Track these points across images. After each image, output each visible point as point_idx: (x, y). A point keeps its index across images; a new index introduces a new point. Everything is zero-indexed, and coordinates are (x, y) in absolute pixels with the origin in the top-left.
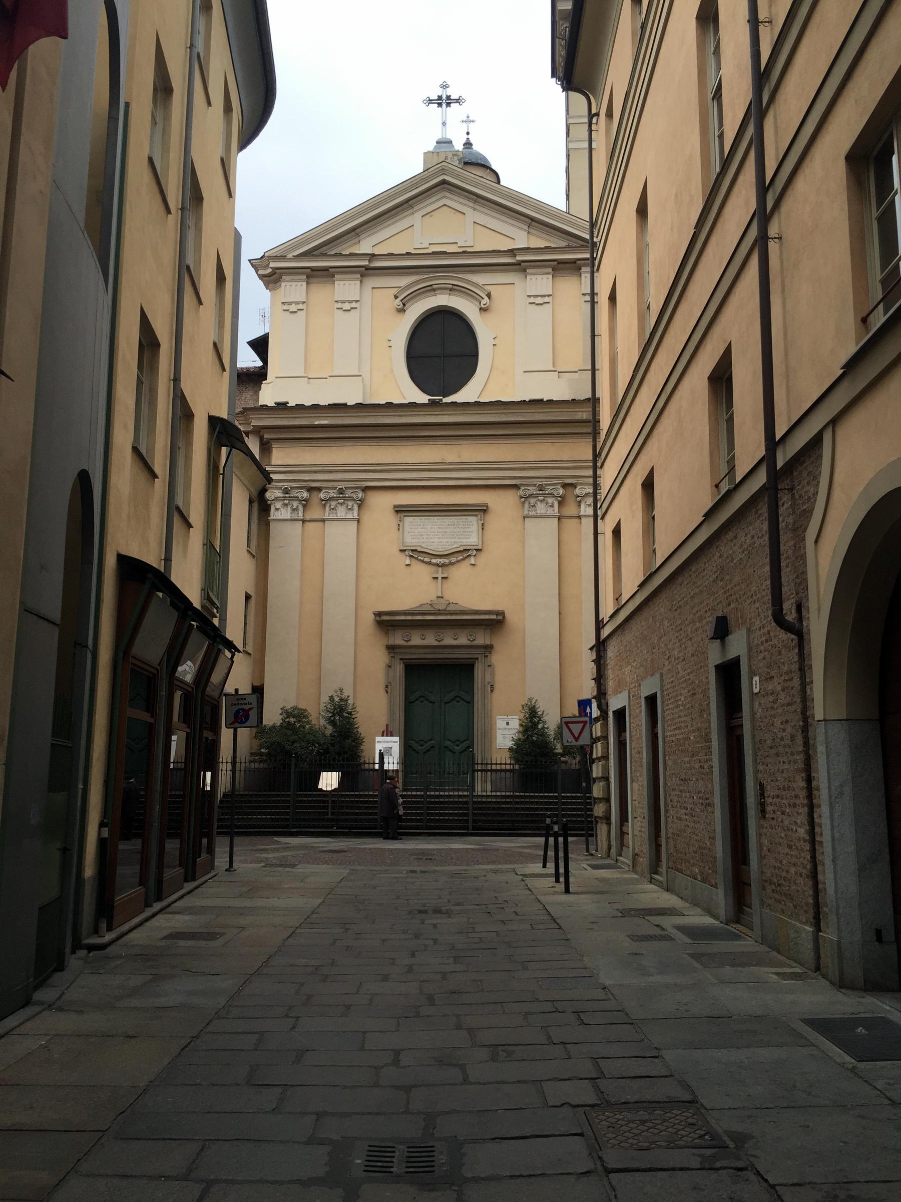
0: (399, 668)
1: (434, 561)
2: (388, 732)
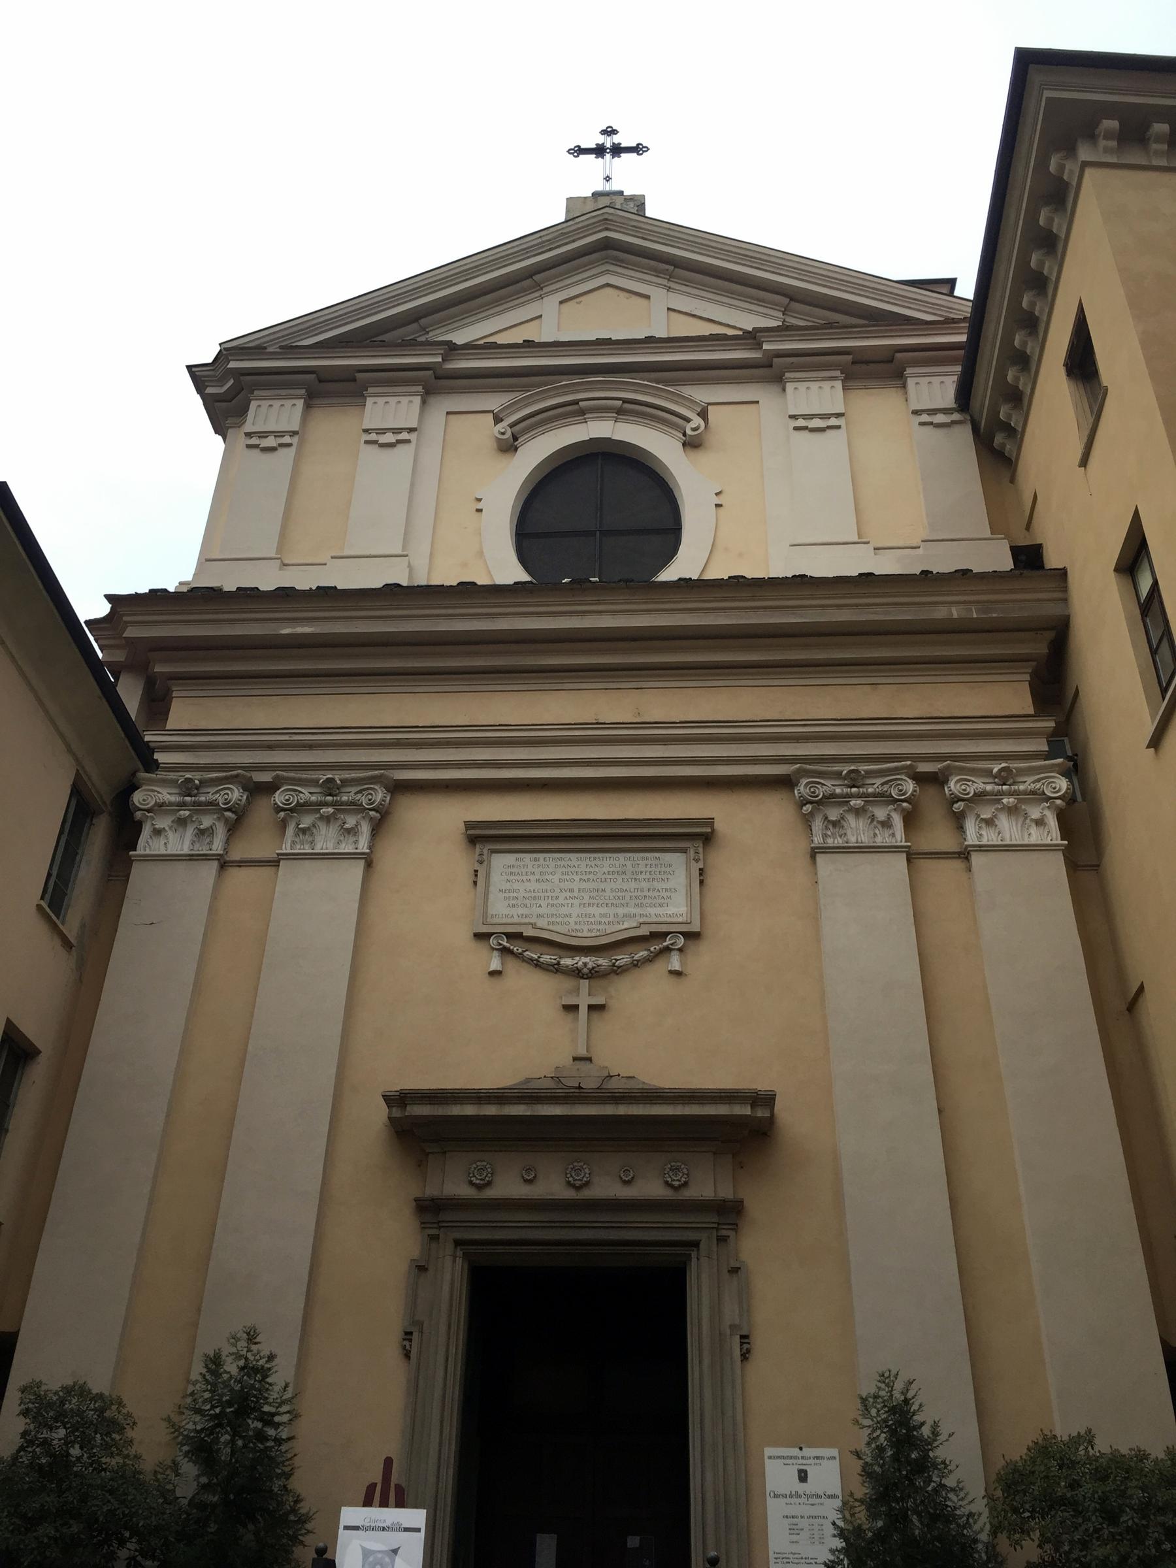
0: (451, 1275)
1: (567, 962)
2: (386, 1492)
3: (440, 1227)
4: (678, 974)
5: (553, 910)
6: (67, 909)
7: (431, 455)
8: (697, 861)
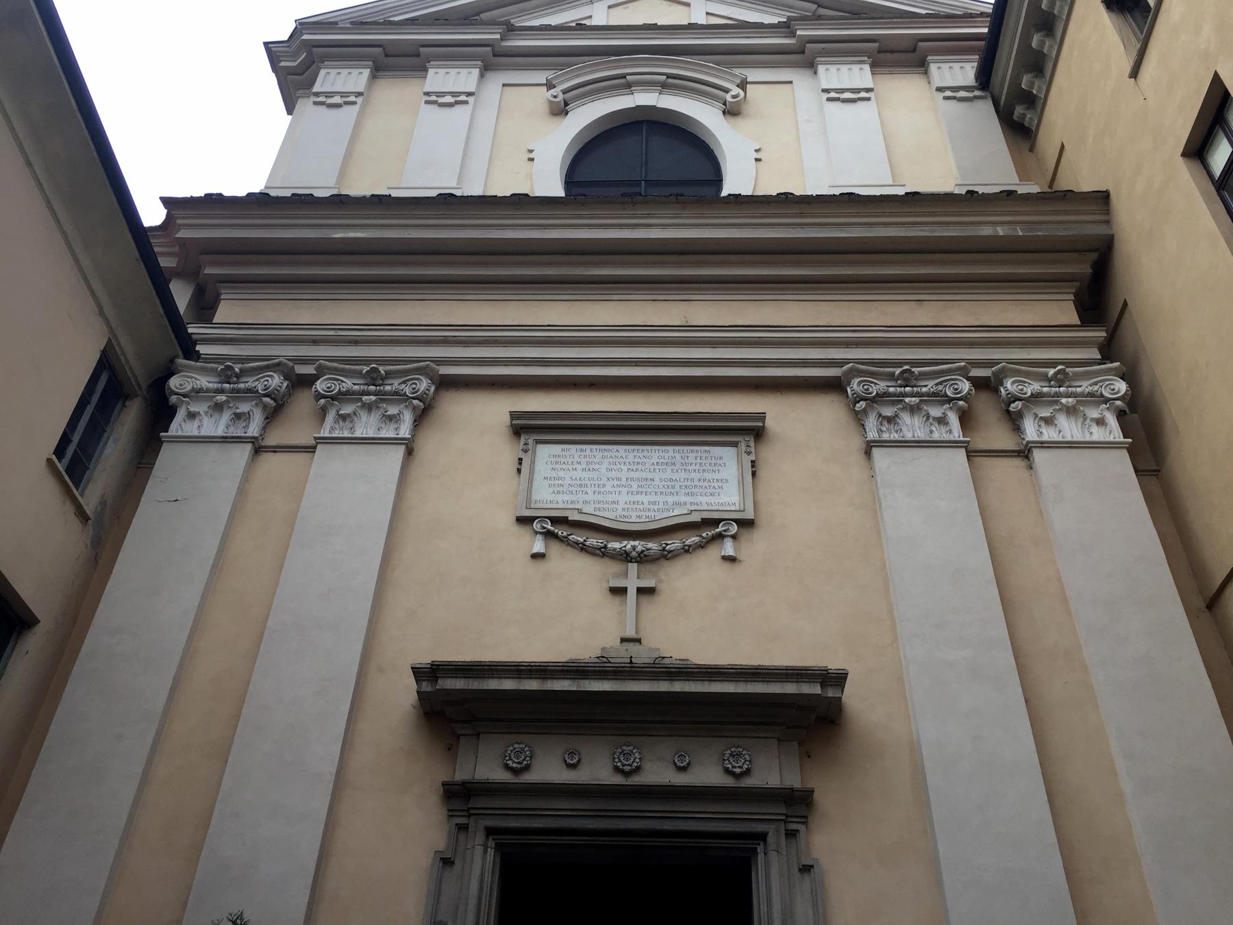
0: (481, 863)
1: (615, 545)
3: (469, 816)
4: (731, 559)
5: (600, 497)
6: (89, 481)
7: (487, 116)
8: (749, 453)
